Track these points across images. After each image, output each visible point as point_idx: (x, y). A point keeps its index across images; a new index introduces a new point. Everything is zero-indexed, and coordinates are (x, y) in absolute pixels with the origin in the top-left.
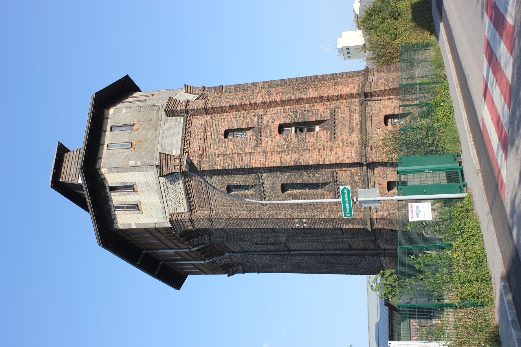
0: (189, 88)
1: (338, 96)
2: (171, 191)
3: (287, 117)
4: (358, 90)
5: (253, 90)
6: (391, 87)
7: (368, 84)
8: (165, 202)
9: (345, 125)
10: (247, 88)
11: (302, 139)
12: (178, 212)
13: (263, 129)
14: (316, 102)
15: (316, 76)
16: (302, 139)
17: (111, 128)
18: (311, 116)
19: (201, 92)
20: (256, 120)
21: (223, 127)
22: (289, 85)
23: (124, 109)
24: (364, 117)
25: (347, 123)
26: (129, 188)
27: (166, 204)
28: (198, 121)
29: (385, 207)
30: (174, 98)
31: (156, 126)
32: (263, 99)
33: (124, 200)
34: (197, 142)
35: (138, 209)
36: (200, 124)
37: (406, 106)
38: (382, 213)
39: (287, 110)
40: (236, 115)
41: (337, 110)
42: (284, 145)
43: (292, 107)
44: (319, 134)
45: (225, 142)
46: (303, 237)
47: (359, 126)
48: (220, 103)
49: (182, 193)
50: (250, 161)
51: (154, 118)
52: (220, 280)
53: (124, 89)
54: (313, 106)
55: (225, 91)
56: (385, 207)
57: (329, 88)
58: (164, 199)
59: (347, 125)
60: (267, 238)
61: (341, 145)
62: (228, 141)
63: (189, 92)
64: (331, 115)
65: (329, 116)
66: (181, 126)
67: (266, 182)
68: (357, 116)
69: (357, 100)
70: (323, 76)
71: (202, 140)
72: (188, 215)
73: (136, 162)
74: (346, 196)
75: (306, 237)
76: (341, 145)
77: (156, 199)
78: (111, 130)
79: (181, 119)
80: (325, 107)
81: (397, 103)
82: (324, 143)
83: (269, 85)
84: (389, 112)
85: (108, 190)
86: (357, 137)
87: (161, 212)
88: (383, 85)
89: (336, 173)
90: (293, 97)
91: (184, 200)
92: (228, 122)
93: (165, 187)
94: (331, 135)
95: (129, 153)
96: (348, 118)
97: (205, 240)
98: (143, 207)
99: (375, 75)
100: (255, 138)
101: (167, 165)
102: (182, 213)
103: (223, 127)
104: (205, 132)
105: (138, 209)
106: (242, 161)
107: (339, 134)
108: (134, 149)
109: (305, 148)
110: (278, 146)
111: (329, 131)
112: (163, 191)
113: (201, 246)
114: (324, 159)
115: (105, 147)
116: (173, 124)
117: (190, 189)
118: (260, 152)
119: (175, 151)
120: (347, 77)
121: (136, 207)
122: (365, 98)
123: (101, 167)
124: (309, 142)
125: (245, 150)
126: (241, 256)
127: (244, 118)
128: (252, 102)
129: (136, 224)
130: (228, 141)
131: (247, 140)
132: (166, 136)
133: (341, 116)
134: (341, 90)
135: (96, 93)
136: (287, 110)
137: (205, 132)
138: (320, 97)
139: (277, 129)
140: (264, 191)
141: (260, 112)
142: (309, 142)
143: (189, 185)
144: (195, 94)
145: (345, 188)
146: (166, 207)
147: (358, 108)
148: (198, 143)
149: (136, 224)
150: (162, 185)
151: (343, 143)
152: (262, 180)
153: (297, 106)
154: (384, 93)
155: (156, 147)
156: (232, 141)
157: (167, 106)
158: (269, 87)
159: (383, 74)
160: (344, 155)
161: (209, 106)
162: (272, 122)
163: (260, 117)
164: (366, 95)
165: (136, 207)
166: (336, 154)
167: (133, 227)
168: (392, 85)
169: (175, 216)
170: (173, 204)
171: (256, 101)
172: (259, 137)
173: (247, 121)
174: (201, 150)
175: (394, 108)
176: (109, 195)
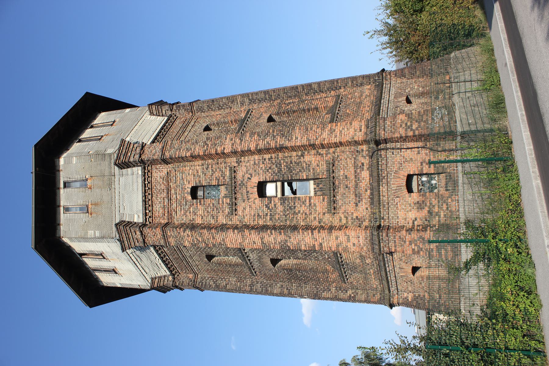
1: (335, 143)
4: (366, 133)
5: (231, 108)
6: (417, 133)
8: (141, 269)
9: (349, 189)
10: (223, 105)
11: (290, 207)
12: (159, 275)
13: (238, 189)
14: (305, 150)
16: (290, 207)
17: (65, 183)
18: (300, 171)
20: (228, 173)
21: (189, 182)
22: (276, 99)
24: (377, 178)
25: (352, 185)
27: (143, 271)
28: (159, 173)
29: (410, 289)
37: (440, 162)
38: (406, 295)
39: (267, 160)
40: (203, 165)
41: (336, 162)
43: (273, 155)
44: (312, 201)
45: (193, 204)
47: (369, 191)
50: (223, 240)
51: (107, 173)
53: (90, 107)
54: (302, 155)
56: (410, 289)
57: (323, 129)
58: (139, 267)
59: (352, 189)
62: (197, 204)
63: (155, 113)
64: (328, 171)
66: (140, 180)
67: (251, 255)
68: (365, 174)
69: (365, 147)
70: (319, 84)
71: (166, 200)
72: (171, 278)
73: (95, 232)
78: (65, 187)
79: (138, 170)
80: (318, 158)
81: (426, 154)
82: (321, 216)
83: (249, 100)
84: (412, 169)
86: (367, 209)
88: (404, 125)
89: (340, 254)
90: (273, 145)
91: (162, 265)
92: (194, 175)
94: (329, 203)
99: (393, 82)
102: (165, 276)
103: (189, 182)
106: (214, 238)
107: (340, 203)
108: (91, 214)
110: (259, 215)
111: (326, 197)
112: (135, 260)
114: (321, 244)
115: (62, 209)
116: (130, 177)
117: (164, 256)
119: (136, 216)
120: (353, 86)
122: (377, 146)
123: (62, 236)
125: (217, 217)
127: (212, 170)
128: (219, 150)
130: (197, 204)
131: (219, 203)
132: (123, 196)
133: (342, 173)
134: (341, 132)
136: (267, 160)
137: (169, 190)
138: (310, 145)
139: (256, 189)
140: (251, 263)
141: (232, 161)
142: (299, 211)
143: (162, 252)
144: (163, 116)
146: (144, 273)
147: (366, 161)
148: (162, 205)
150: (131, 255)
151: (347, 218)
152: (246, 253)
153: (280, 154)
154: (405, 140)
155: (114, 212)
156: (201, 204)
157: (118, 157)
158: (250, 103)
159: (405, 80)
160: (348, 240)
161: (167, 155)
162: (249, 178)
163: (233, 171)
164: (377, 143)
166: (337, 238)
168: (417, 129)
169: (157, 280)
170: (151, 269)
171: (224, 148)
173: (217, 174)
175: (422, 165)
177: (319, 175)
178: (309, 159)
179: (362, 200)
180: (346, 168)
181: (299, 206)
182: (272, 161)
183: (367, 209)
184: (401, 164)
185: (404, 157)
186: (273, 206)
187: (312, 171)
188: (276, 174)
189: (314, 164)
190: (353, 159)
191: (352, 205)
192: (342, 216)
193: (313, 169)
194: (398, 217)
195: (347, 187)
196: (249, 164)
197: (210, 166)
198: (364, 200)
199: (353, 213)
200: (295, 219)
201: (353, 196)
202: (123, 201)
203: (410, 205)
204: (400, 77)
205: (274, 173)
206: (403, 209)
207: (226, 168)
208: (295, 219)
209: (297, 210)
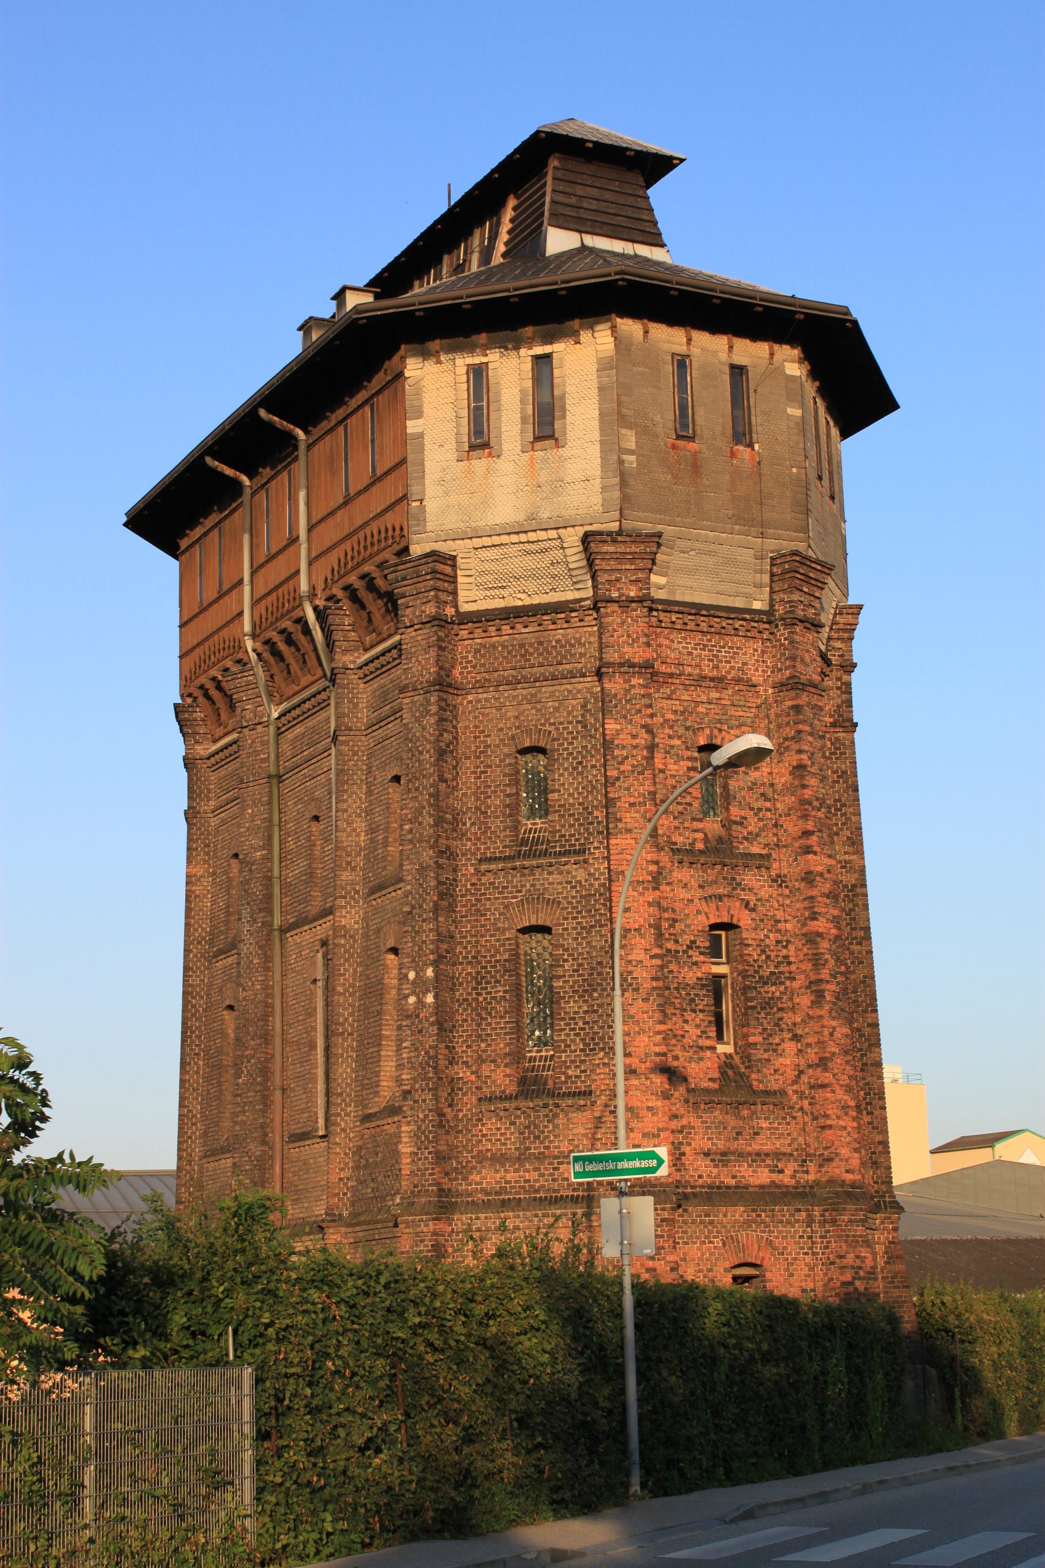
0: (850, 619)
2: (530, 562)
3: (763, 951)
7: (861, 1216)
8: (496, 540)
12: (460, 579)
15: (878, 1044)
16: (693, 1000)
19: (834, 660)
20: (755, 849)
23: (798, 413)
25: (741, 1144)
26: (545, 424)
27: (487, 541)
30: (829, 581)
31: (749, 517)
32: (821, 875)
33: (504, 399)
34: (690, 654)
35: (472, 447)
36: (744, 664)
39: (784, 952)
42: (676, 941)
44: (708, 1053)
46: (353, 986)
47: (733, 1182)
48: (811, 734)
49: (523, 596)
50: (629, 831)
52: (159, 677)
55: (837, 739)
58: (505, 539)
59: (734, 1146)
60: (349, 864)
61: (675, 1124)
62: (689, 759)
65: (761, 1087)
67: (556, 877)
68: (762, 1176)
73: (631, 452)
74: (637, 1164)
75: (352, 995)
76: (675, 1124)
77: (506, 510)
80: (791, 1074)
83: (854, 886)
85: (539, 350)
86: (700, 1177)
87: (462, 525)
88: (858, 1263)
93: (547, 544)
94: (707, 1091)
95: (659, 430)
96: (756, 1147)
97: (345, 651)
98: (480, 464)
100: (700, 846)
101: (620, 558)
104: (719, 682)
105: (472, 447)
106: (632, 805)
108: (674, 447)
109: (670, 1011)
110: (675, 921)
112: (532, 536)
113: (318, 635)
118: (657, 863)
121: (479, 440)
124: (686, 1021)
126: (263, 761)
127: (760, 810)
129: (421, 436)
130: (689, 759)
132: (710, 553)
133: (764, 1124)
134: (845, 1128)
135: (855, 323)
136: (784, 952)
137: (719, 682)
142: (686, 1021)
145: (660, 1162)
146: (478, 542)
149: (421, 436)
150: (553, 534)
156: (689, 769)
165: (479, 440)
167: (409, 423)
169: (448, 570)
170: (487, 566)
172: (702, 860)
174: (663, 668)
176: (523, 351)
177: (759, 1071)
178: (787, 1052)
179: (716, 1166)
180: (771, 1133)
181: (698, 1021)
182: (782, 963)
183: (700, 1177)
184: (783, 1254)
185: (795, 1259)
186: (694, 959)
187: (766, 1056)
188: (757, 972)
189: (779, 1062)
190: (789, 1151)
191: (708, 1145)
192: (684, 1122)
193: (768, 1060)
194: (687, 1243)
195: (737, 1134)
196: (776, 905)
197: (768, 804)
198: (715, 1171)
199: (689, 1144)
200: (673, 1011)
201: (721, 1145)
202: (702, 552)
203: (711, 1270)
204: (886, 1252)
205: (760, 967)
206: (703, 1255)
207: (766, 845)
208: (673, 1011)
209: (689, 1015)
